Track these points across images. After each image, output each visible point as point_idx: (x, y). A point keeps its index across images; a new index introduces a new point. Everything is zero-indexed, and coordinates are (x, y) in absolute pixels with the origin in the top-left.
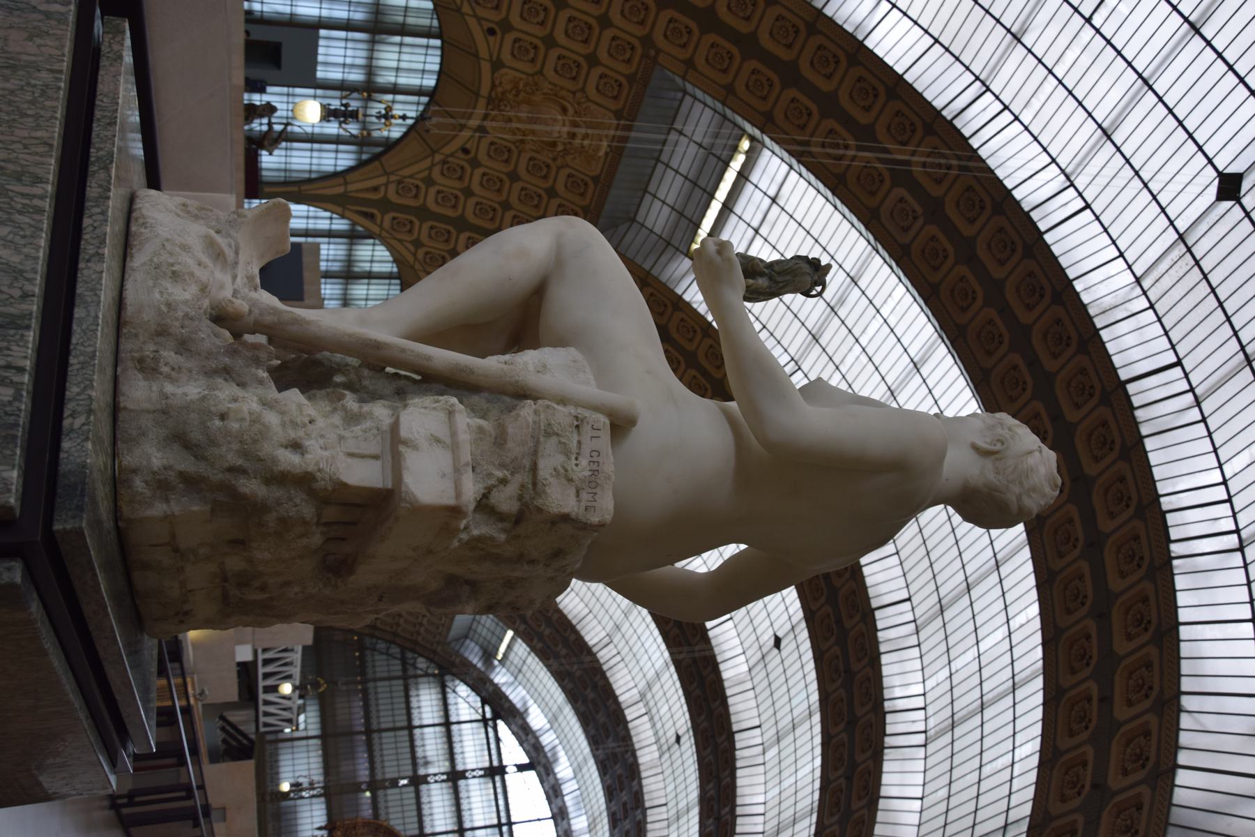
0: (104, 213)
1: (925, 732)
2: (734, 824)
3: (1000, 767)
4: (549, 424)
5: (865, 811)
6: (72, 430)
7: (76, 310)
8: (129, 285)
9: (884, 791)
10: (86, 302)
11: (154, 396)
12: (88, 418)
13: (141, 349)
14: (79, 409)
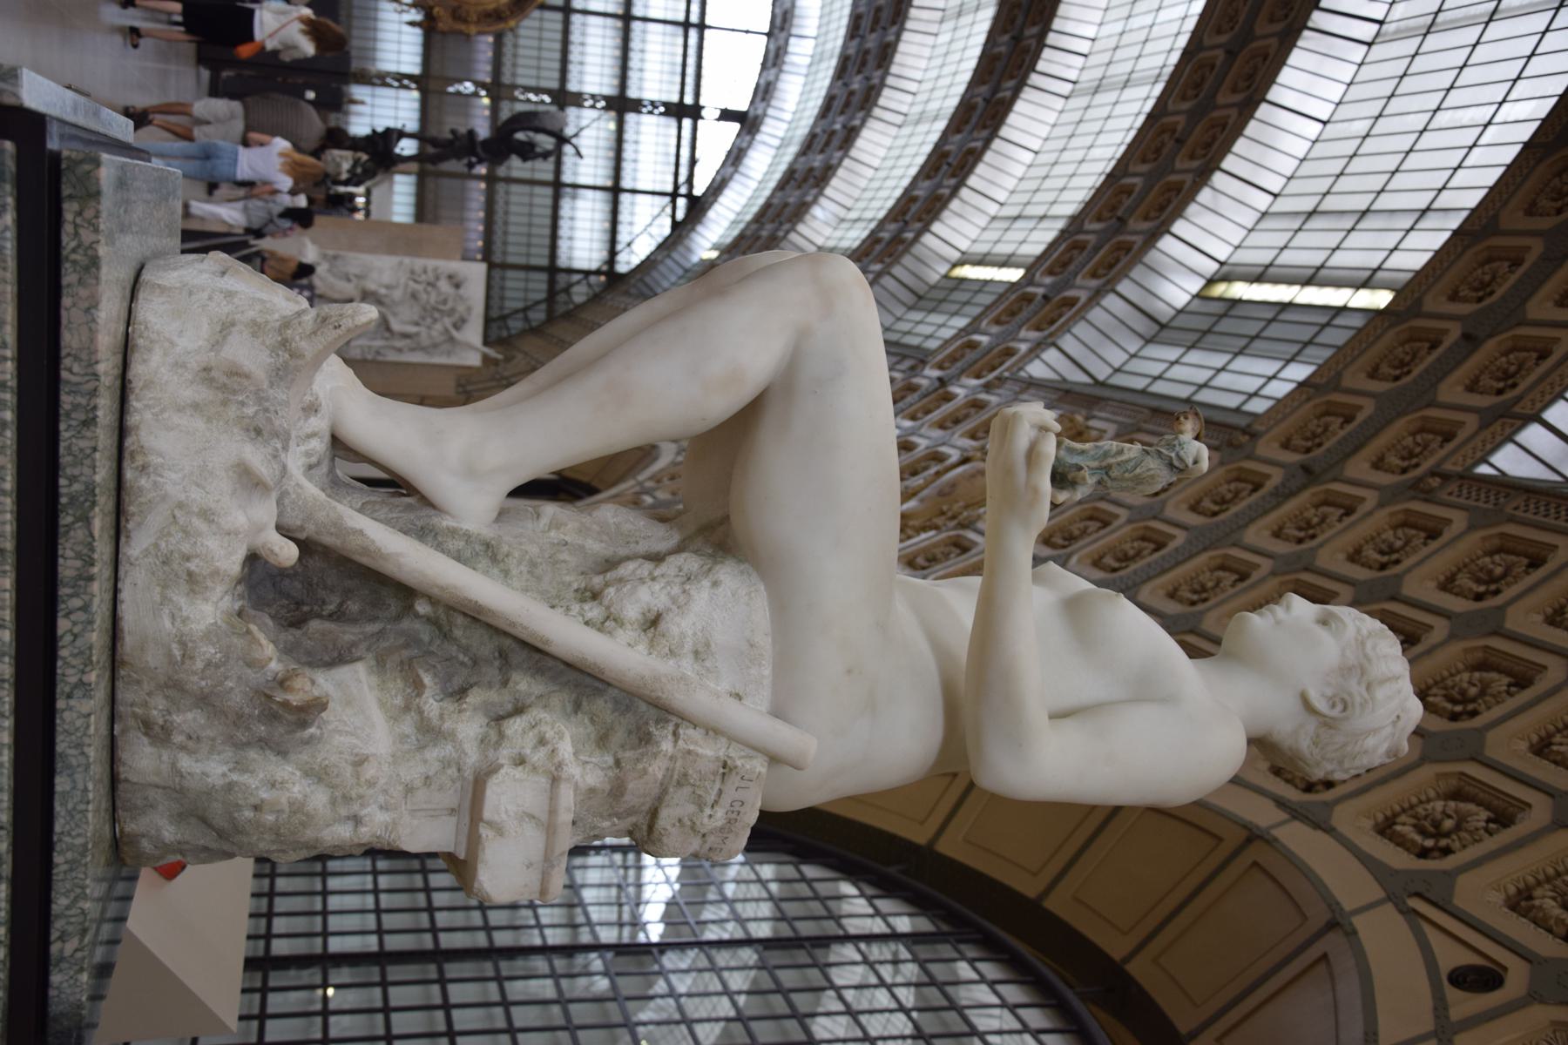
0: (85, 608)
1: (1381, 23)
2: (1037, 56)
3: (1465, 122)
4: (685, 775)
5: (1234, 112)
6: (62, 959)
7: (58, 780)
8: (126, 594)
9: (1275, 94)
10: (70, 767)
11: (165, 768)
12: (81, 941)
13: (145, 705)
14: (70, 929)
